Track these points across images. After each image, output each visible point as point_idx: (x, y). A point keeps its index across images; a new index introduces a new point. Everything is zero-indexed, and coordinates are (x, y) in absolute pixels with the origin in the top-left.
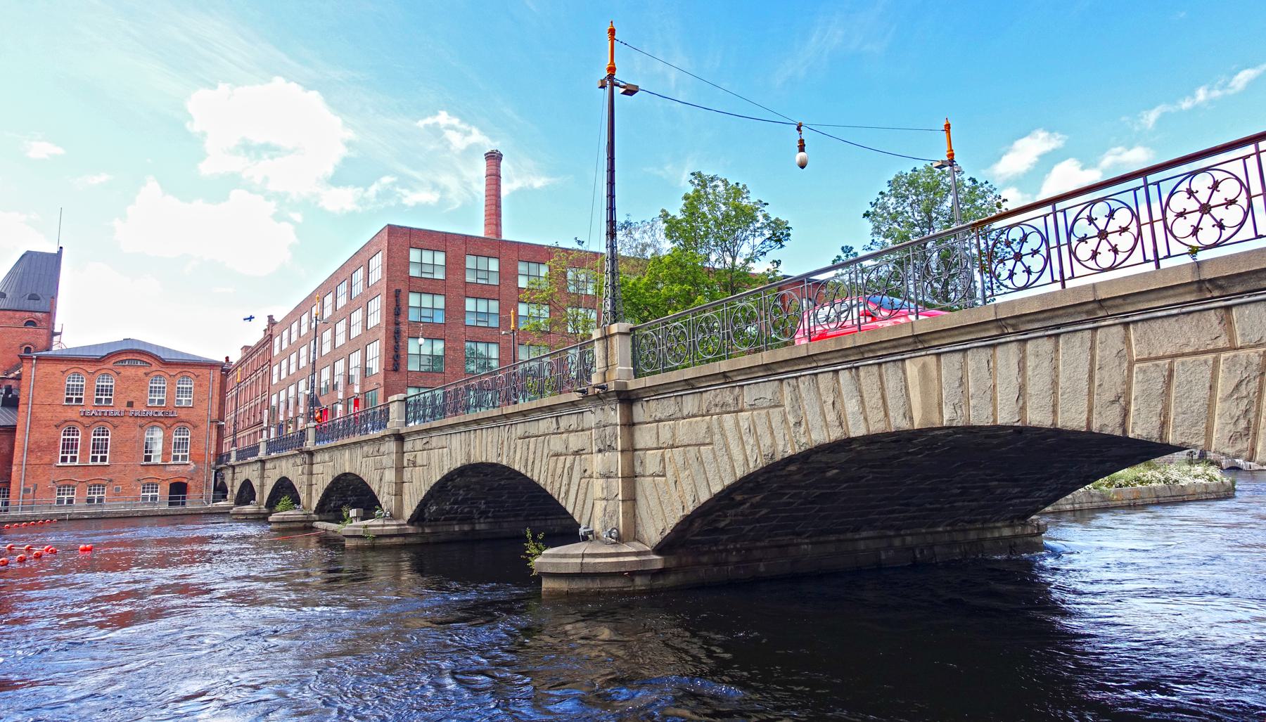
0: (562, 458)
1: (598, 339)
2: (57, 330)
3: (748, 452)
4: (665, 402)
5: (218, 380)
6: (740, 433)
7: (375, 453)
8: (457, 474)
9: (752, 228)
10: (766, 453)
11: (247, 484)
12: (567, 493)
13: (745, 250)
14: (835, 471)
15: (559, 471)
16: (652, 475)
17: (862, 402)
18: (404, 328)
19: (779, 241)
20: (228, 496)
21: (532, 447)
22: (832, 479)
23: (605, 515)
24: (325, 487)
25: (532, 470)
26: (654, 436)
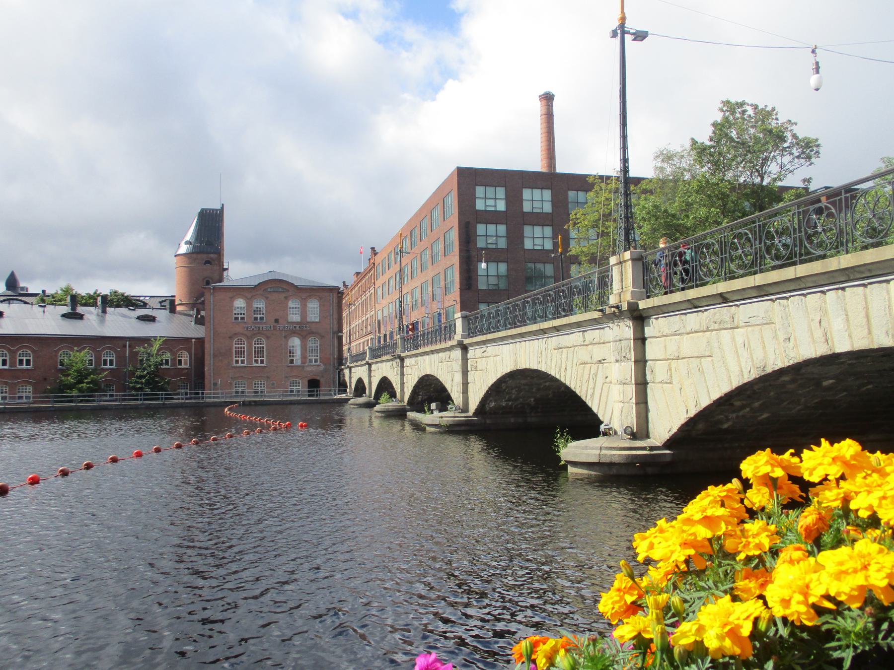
0: (588, 366)
1: (614, 265)
2: (225, 267)
3: (743, 365)
5: (335, 301)
6: (736, 348)
7: (447, 359)
9: (781, 148)
10: (758, 366)
11: (360, 381)
12: (592, 395)
13: (773, 168)
14: (831, 381)
15: (586, 377)
16: (661, 382)
17: (847, 320)
18: (474, 253)
19: (809, 158)
20: (348, 390)
21: (564, 356)
22: (829, 388)
23: (621, 415)
25: (565, 376)
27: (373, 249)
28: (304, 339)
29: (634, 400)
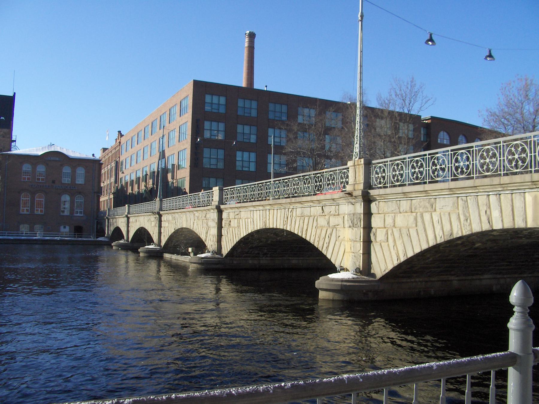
1: (351, 166)
4: (390, 203)
8: (255, 233)
14: (480, 244)
24: (170, 235)
26: (383, 221)
27: (120, 132)
28: (72, 196)
29: (361, 252)
